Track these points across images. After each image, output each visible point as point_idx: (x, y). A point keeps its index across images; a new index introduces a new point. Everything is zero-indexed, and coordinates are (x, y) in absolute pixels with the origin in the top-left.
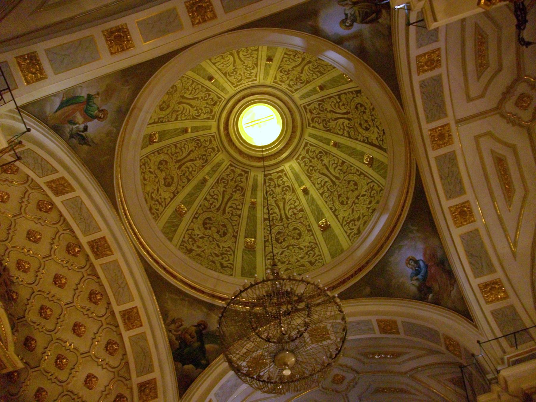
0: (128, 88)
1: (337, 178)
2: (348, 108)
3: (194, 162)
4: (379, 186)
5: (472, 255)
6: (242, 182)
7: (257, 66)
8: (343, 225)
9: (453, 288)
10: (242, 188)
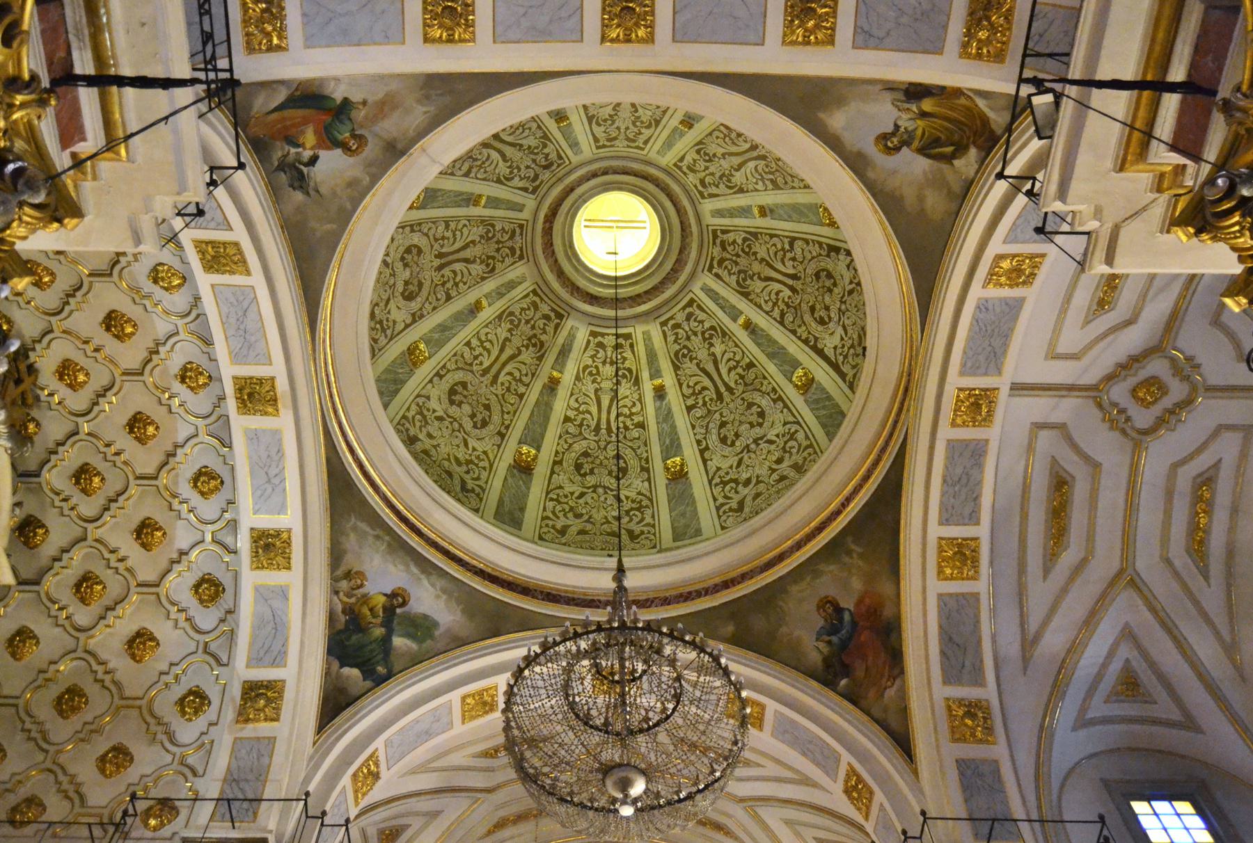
0: (425, 109)
1: (730, 390)
2: (800, 268)
3: (469, 266)
4: (807, 437)
5: (950, 639)
6: (545, 332)
7: (657, 126)
8: (714, 482)
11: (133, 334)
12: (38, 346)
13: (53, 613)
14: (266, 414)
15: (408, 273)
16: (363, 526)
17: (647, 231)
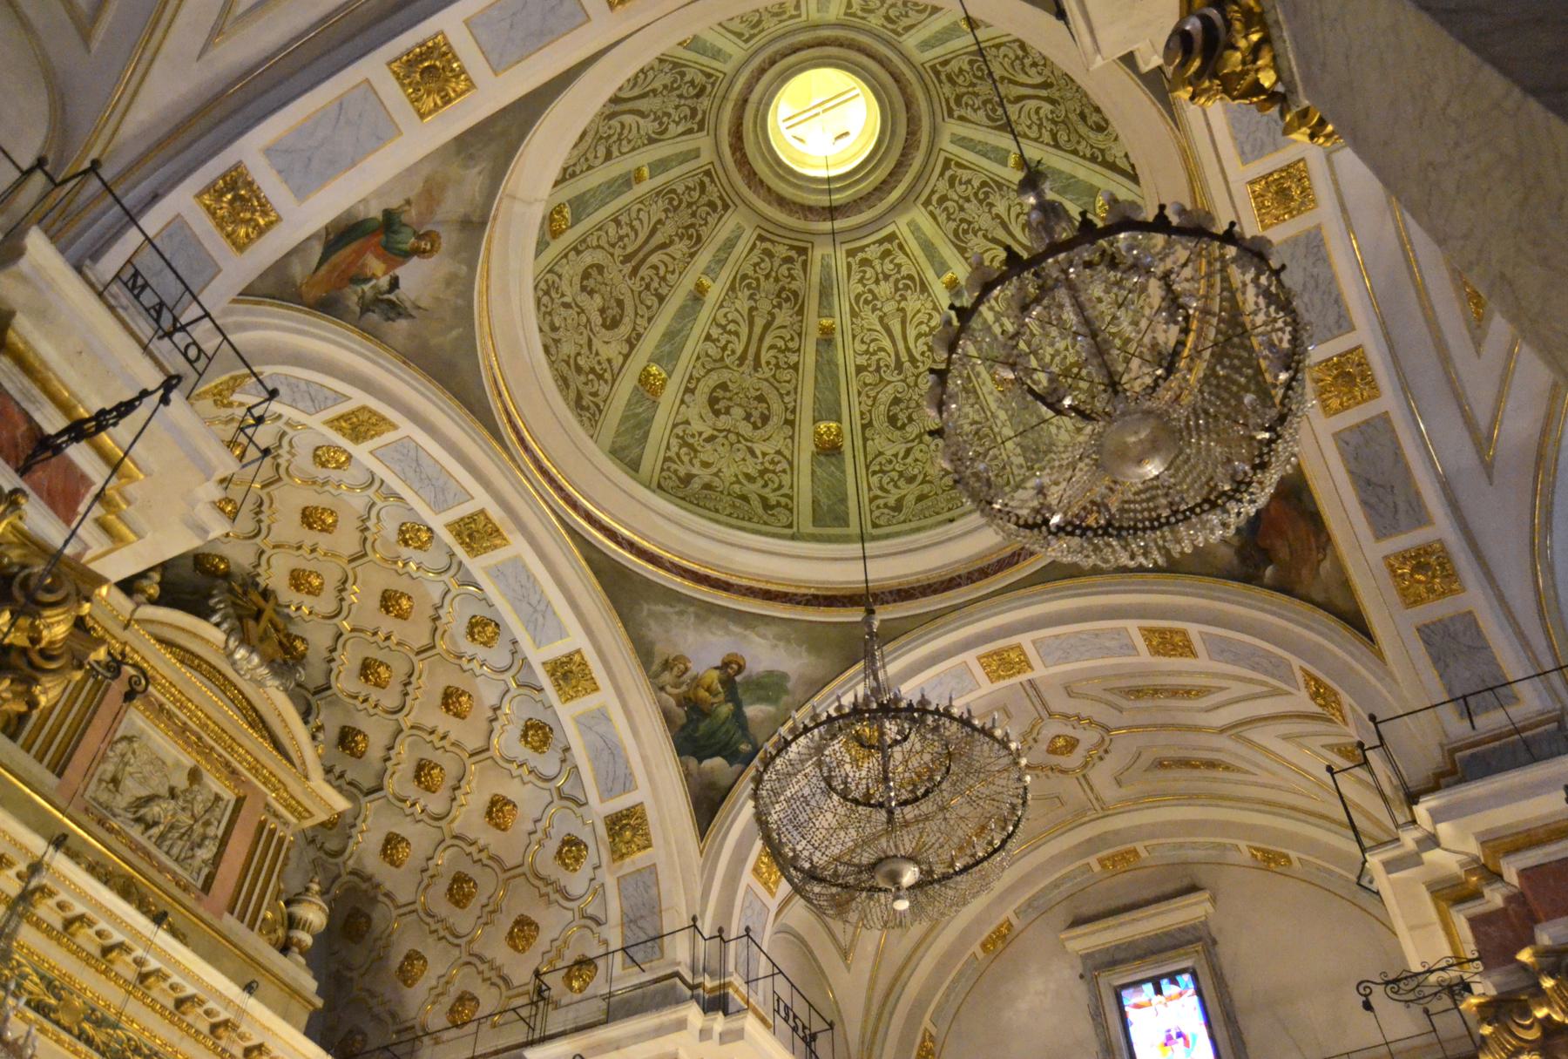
5: (1369, 483)
6: (793, 278)
9: (1325, 556)
10: (795, 294)
11: (336, 521)
12: (260, 570)
13: (408, 811)
14: (496, 547)
15: (598, 300)
16: (660, 608)
17: (861, 99)
